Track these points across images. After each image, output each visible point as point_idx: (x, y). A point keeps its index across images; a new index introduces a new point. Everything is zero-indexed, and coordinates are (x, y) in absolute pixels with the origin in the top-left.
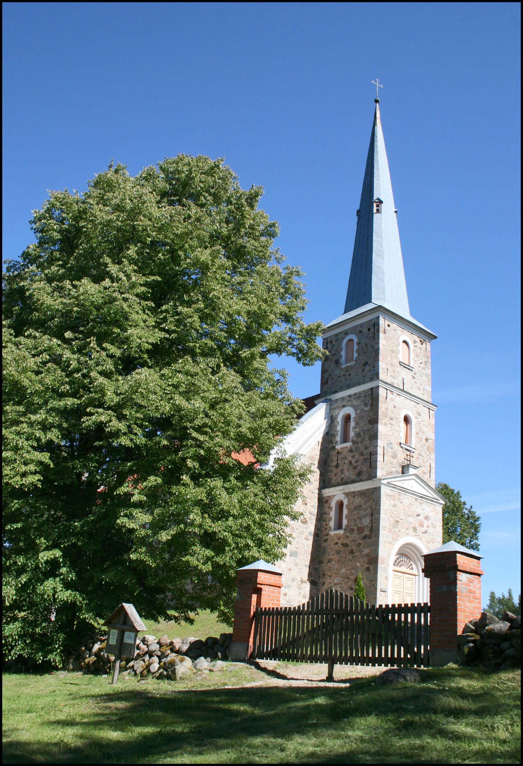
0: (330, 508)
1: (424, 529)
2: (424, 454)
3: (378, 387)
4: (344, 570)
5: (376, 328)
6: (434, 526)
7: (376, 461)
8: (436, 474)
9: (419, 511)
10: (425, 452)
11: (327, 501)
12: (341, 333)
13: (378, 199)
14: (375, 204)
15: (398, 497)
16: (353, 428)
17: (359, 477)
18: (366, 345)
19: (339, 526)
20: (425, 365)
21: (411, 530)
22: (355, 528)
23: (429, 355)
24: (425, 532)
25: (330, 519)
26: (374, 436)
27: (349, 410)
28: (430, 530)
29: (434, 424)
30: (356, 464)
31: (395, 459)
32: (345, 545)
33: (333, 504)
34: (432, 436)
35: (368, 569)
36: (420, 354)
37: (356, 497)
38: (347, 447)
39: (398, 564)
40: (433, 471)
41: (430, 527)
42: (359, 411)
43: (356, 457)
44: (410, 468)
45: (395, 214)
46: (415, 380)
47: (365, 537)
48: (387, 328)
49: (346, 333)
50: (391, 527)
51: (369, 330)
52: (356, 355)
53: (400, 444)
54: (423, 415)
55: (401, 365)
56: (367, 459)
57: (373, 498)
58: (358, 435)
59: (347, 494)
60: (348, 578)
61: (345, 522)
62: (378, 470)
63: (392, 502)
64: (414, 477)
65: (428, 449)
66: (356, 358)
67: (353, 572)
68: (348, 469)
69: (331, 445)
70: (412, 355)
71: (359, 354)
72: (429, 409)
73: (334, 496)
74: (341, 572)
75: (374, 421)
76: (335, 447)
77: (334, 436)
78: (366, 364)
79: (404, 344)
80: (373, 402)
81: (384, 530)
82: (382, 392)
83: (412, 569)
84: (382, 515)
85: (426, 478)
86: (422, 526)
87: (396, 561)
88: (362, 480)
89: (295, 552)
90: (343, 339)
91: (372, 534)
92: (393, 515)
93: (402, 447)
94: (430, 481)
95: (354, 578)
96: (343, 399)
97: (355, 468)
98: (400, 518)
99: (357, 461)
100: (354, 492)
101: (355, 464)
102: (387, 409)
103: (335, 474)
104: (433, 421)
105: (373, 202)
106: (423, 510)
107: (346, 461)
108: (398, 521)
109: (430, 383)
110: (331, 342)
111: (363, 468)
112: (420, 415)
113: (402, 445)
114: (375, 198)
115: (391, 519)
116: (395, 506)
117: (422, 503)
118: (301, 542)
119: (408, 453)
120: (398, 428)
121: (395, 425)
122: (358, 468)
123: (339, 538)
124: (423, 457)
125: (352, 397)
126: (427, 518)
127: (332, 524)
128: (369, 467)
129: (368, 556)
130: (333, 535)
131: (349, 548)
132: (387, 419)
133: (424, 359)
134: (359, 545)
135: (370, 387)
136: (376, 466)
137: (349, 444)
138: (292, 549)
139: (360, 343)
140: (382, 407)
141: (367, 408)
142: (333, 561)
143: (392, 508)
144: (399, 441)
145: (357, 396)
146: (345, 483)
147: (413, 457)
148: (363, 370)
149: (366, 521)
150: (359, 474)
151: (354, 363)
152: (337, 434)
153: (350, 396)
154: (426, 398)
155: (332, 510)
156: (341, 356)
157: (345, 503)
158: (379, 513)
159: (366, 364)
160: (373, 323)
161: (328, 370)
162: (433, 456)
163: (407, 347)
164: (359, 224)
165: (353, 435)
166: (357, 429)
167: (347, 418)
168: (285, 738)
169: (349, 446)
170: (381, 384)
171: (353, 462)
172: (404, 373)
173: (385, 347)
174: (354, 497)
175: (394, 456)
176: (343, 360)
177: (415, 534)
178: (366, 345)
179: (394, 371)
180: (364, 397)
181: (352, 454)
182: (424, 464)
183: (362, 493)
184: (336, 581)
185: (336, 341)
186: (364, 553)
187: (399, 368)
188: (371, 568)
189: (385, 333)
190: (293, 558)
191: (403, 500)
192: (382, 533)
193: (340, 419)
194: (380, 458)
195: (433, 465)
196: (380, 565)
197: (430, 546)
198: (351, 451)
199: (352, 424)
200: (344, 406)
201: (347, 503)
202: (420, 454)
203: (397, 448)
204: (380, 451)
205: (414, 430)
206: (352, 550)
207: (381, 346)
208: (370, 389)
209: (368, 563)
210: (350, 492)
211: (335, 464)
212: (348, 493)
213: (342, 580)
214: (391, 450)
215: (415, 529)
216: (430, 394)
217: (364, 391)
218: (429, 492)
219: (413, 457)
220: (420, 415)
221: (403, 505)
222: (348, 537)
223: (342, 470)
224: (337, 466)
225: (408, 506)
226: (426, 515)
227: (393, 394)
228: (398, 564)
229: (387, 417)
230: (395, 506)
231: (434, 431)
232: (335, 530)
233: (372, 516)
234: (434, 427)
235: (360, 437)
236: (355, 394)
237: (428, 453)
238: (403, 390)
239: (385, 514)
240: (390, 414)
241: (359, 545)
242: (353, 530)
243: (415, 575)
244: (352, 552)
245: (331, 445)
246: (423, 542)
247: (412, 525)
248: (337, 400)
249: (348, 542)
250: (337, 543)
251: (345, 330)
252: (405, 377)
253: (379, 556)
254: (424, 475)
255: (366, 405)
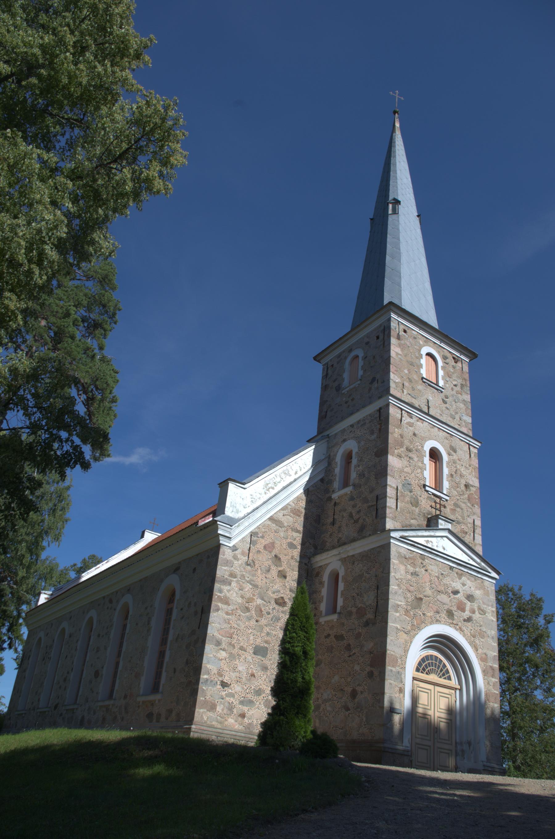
0: (322, 583)
1: (467, 614)
2: (463, 505)
3: (388, 405)
4: (336, 678)
5: (386, 333)
6: (483, 612)
7: (385, 507)
8: (483, 535)
9: (457, 585)
10: (464, 503)
11: (318, 574)
12: (344, 351)
13: (394, 199)
14: (390, 206)
15: (420, 561)
16: (355, 467)
17: (362, 533)
18: (374, 357)
19: (333, 610)
20: (461, 388)
21: (444, 615)
22: (354, 610)
23: (467, 376)
24: (469, 620)
25: (321, 601)
26: (382, 472)
27: (352, 445)
28: (477, 616)
29: (477, 466)
30: (358, 516)
31: (416, 507)
32: (339, 638)
33: (326, 578)
34: (475, 482)
35: (371, 675)
36: (453, 373)
37: (356, 563)
38: (346, 494)
39: (424, 669)
40: (479, 531)
41: (477, 612)
42: (363, 443)
43: (358, 506)
44: (440, 521)
45: (418, 218)
46: (447, 405)
47: (367, 624)
48: (402, 333)
49: (350, 350)
50: (409, 608)
51: (378, 338)
52: (361, 373)
53: (425, 486)
54: (459, 452)
55: (424, 382)
56: (372, 506)
57: (380, 560)
58: (361, 475)
59: (344, 561)
60: (342, 690)
61: (340, 602)
62: (387, 519)
63: (411, 569)
64: (446, 534)
65: (469, 499)
66: (362, 376)
67: (349, 680)
68: (347, 525)
69: (327, 495)
70: (441, 373)
71: (365, 371)
72: (469, 445)
73: (327, 565)
74: (333, 681)
75: (382, 452)
76: (331, 497)
77: (330, 482)
78: (373, 380)
79: (428, 357)
80: (381, 426)
81: (397, 611)
82: (392, 411)
83: (449, 678)
84: (393, 587)
85: (468, 539)
86: (463, 610)
87: (420, 664)
88: (364, 537)
89: (262, 647)
90: (346, 358)
91: (375, 618)
92: (412, 589)
93: (427, 491)
94: (475, 545)
95: (350, 690)
96: (344, 431)
97: (356, 522)
98: (425, 594)
99: (359, 512)
100: (353, 556)
101: (356, 517)
102: (402, 436)
103: (331, 535)
104: (475, 462)
105: (388, 204)
106: (464, 585)
107: (345, 514)
108: (421, 599)
109: (469, 412)
110: (332, 366)
111: (367, 520)
112: (455, 451)
113: (427, 488)
114: (391, 198)
115: (409, 595)
116: (414, 574)
117: (461, 575)
118: (274, 633)
119: (438, 500)
120: (420, 464)
121: (416, 459)
122: (361, 521)
123: (332, 628)
124: (462, 509)
125: (355, 427)
126: (470, 598)
127: (323, 607)
128: (374, 517)
129: (371, 653)
130: (323, 623)
131: (345, 641)
132: (402, 449)
133: (460, 381)
134: (358, 635)
135: (378, 408)
136: (385, 513)
137: (348, 490)
138: (257, 643)
139: (366, 357)
140: (394, 433)
141: (374, 437)
142: (323, 664)
143: (409, 577)
144: (422, 483)
145: (361, 423)
146: (341, 544)
147: (445, 507)
148: (370, 389)
149: (369, 599)
150: (362, 530)
151: (359, 382)
152: (335, 479)
153: (352, 426)
154: (464, 430)
155: (323, 586)
156: (343, 380)
157: (342, 573)
158: (387, 584)
159: (373, 380)
160: (382, 328)
161: (327, 401)
162: (477, 510)
163: (433, 362)
164: (372, 232)
165: (355, 476)
166: (361, 468)
167: (348, 457)
168: (295, 512)
169: (349, 492)
170: (392, 400)
171: (354, 514)
172: (431, 395)
173: (399, 356)
174: (353, 564)
175: (415, 503)
176: (346, 383)
177: (451, 621)
178: (374, 357)
179: (413, 389)
180: (370, 422)
181: (352, 503)
182: (464, 519)
183: (365, 556)
184: (325, 696)
185: (338, 363)
186: (365, 649)
187: (420, 387)
188: (376, 673)
189: (398, 337)
190: (259, 657)
191: (430, 568)
192: (393, 615)
193: (338, 459)
194: (390, 503)
195: (478, 523)
196: (388, 668)
197: (477, 642)
198: (352, 499)
199: (354, 461)
200: (344, 441)
201: (344, 574)
202: (456, 505)
203: (418, 491)
204: (390, 492)
205: (446, 471)
206: (349, 645)
207: (393, 354)
208: (377, 411)
209: (371, 666)
210: (348, 556)
211: (330, 520)
212: (345, 558)
213: (334, 693)
214: (409, 493)
215: (450, 614)
216: (470, 426)
217: (370, 415)
218: (472, 559)
219: (445, 507)
220: (455, 451)
221: (430, 574)
222: (343, 624)
223: (340, 527)
224: (333, 523)
225: (438, 578)
226: (469, 593)
227: (411, 417)
228: (424, 669)
229: (402, 446)
230: (414, 574)
231: (477, 475)
232: (327, 614)
233: (378, 588)
234: (477, 470)
235: (364, 476)
236: (358, 422)
237: (469, 504)
238: (428, 414)
239: (398, 585)
240: (407, 443)
241: (358, 635)
242: (350, 613)
243: (456, 689)
244: (348, 648)
245: (327, 495)
246: (464, 636)
247: (446, 607)
248: (336, 434)
249: (343, 632)
250: (329, 635)
251: (349, 347)
252: (430, 398)
253: (388, 652)
254: (463, 535)
255: (372, 433)
